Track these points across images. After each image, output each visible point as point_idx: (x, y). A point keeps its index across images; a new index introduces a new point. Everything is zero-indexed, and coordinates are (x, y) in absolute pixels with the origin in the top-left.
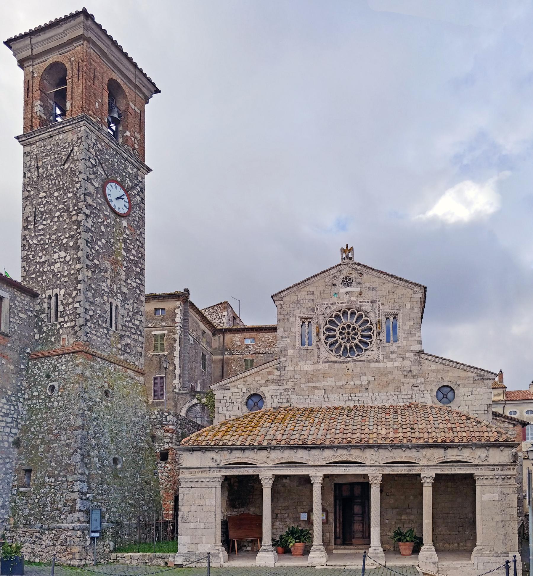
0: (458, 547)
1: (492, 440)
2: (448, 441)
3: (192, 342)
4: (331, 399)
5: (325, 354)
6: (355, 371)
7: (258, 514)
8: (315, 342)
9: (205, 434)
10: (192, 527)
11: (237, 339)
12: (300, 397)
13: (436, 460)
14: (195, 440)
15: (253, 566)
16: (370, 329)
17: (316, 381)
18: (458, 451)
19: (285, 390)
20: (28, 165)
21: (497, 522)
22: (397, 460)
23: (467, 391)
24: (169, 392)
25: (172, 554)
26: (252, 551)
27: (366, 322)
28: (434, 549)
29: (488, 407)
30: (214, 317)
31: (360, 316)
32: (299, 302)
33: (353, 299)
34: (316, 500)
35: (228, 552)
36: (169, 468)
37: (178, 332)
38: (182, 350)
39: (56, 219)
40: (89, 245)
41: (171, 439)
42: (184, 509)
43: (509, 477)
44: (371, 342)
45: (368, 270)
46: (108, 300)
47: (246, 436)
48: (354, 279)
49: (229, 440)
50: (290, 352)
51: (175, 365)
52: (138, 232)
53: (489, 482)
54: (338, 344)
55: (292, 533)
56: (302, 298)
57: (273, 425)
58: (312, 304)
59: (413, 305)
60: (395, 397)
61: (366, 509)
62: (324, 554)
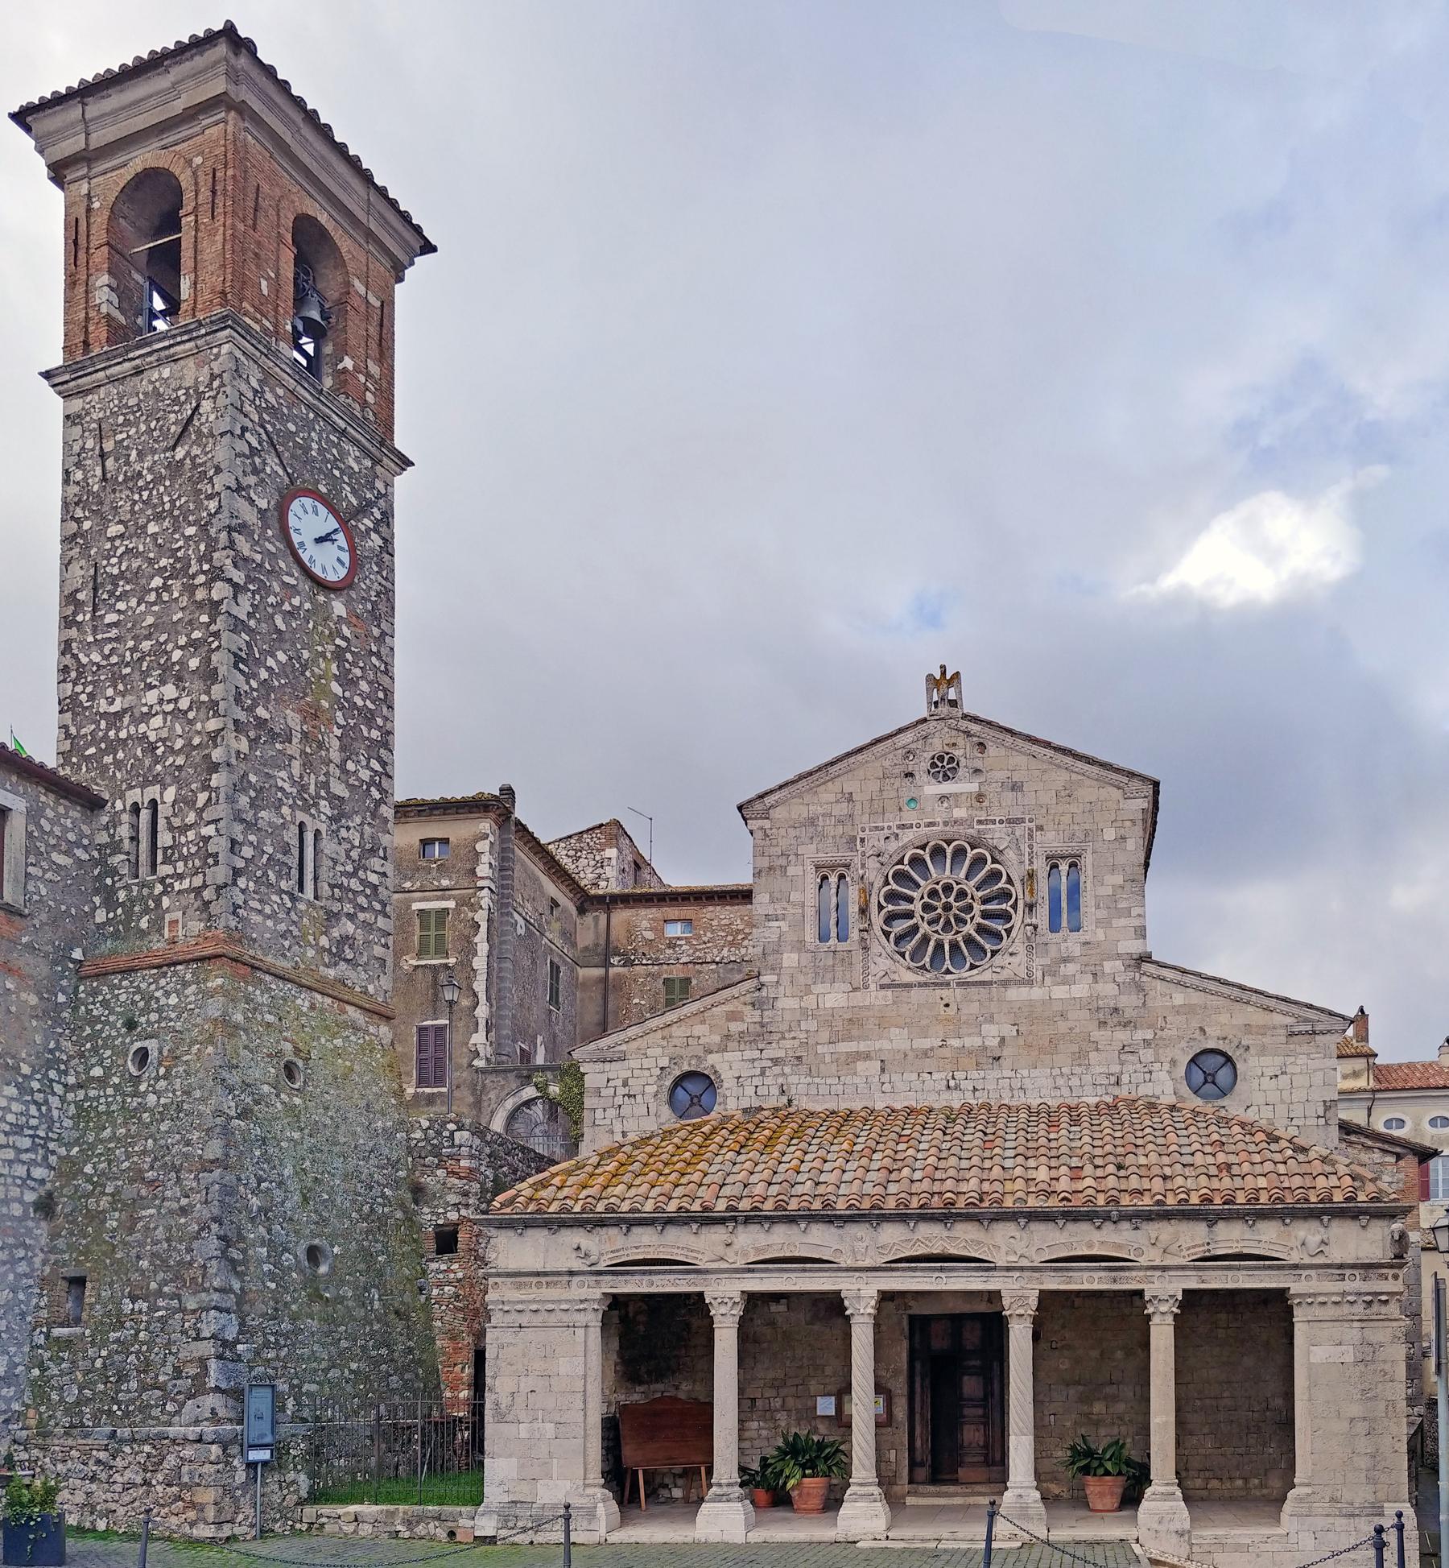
0: (1246, 1488)
1: (1338, 1197)
2: (1217, 1201)
3: (521, 931)
4: (899, 1085)
5: (884, 964)
6: (964, 1011)
7: (702, 1399)
8: (856, 931)
9: (556, 1181)
10: (522, 1435)
11: (645, 924)
12: (817, 1080)
13: (1185, 1253)
14: (531, 1199)
15: (689, 1540)
16: (1005, 895)
17: (859, 1038)
18: (1245, 1227)
19: (776, 1061)
20: (76, 448)
21: (1352, 1420)
22: (1080, 1253)
23: (1271, 1064)
24: (459, 1067)
25: (469, 1508)
26: (686, 1500)
27: (995, 876)
28: (1179, 1493)
29: (1327, 1108)
30: (583, 862)
31: (979, 861)
32: (812, 822)
33: (959, 813)
34: (859, 1361)
35: (620, 1503)
36: (460, 1275)
37: (485, 903)
38: (495, 953)
39: (152, 597)
40: (241, 666)
41: (466, 1194)
42: (500, 1385)
43: (1384, 1298)
44: (1009, 931)
45: (1001, 736)
46: (293, 816)
47: (668, 1186)
48: (962, 760)
49: (623, 1197)
50: (790, 959)
51: (475, 995)
52: (376, 632)
53: (1331, 1312)
54: (919, 936)
55: (794, 1450)
56: (820, 810)
57: (742, 1158)
58: (848, 829)
59: (1122, 831)
60: (1075, 1081)
61: (996, 1386)
62: (881, 1508)
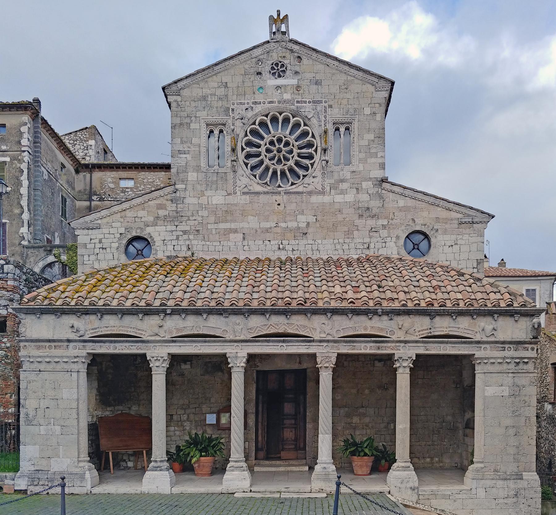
0: (432, 463)
1: (503, 304)
2: (436, 305)
3: (46, 177)
4: (253, 247)
5: (245, 181)
6: (288, 208)
7: (144, 414)
8: (229, 162)
9: (61, 288)
10: (42, 433)
11: (110, 180)
12: (208, 243)
13: (417, 334)
14: (46, 298)
15: (138, 492)
16: (310, 145)
17: (231, 221)
18: (451, 320)
19: (185, 232)
21: (507, 427)
22: (359, 333)
23: (449, 239)
24: (13, 245)
25: (11, 474)
26: (135, 468)
27: (305, 134)
28: (411, 466)
29: (478, 263)
30: (77, 147)
31: (297, 125)
32: (204, 98)
33: (287, 96)
34: (236, 393)
35: (98, 470)
36: (8, 345)
37: (26, 159)
38: (32, 186)
41: (11, 300)
42: (29, 405)
43: (526, 360)
44: (312, 165)
45: (310, 52)
47: (126, 292)
48: (289, 65)
49: (100, 298)
50: (192, 176)
51: (22, 207)
53: (497, 368)
54: (263, 166)
55: (195, 442)
56: (209, 92)
57: (167, 279)
58: (225, 104)
59: (374, 110)
60: (346, 247)
61: (302, 410)
62: (247, 474)
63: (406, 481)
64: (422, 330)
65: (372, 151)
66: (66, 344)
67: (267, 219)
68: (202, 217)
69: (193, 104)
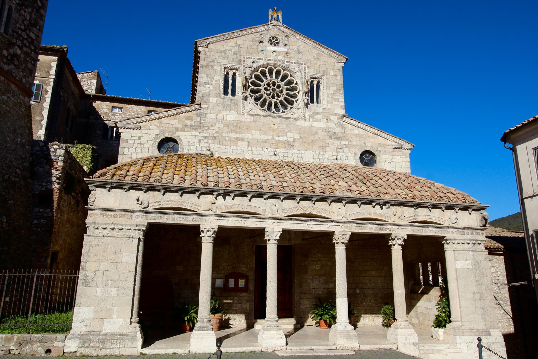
4: (255, 151)
5: (250, 106)
6: (280, 127)
12: (222, 146)
17: (240, 133)
19: (205, 138)
21: (474, 293)
32: (224, 52)
33: (280, 58)
43: (480, 242)
51: (43, 116)
53: (460, 247)
59: (336, 73)
60: (321, 157)
63: (409, 337)
64: (410, 217)
65: (336, 97)
66: (130, 213)
67: (265, 133)
68: (219, 128)
69: (216, 54)
